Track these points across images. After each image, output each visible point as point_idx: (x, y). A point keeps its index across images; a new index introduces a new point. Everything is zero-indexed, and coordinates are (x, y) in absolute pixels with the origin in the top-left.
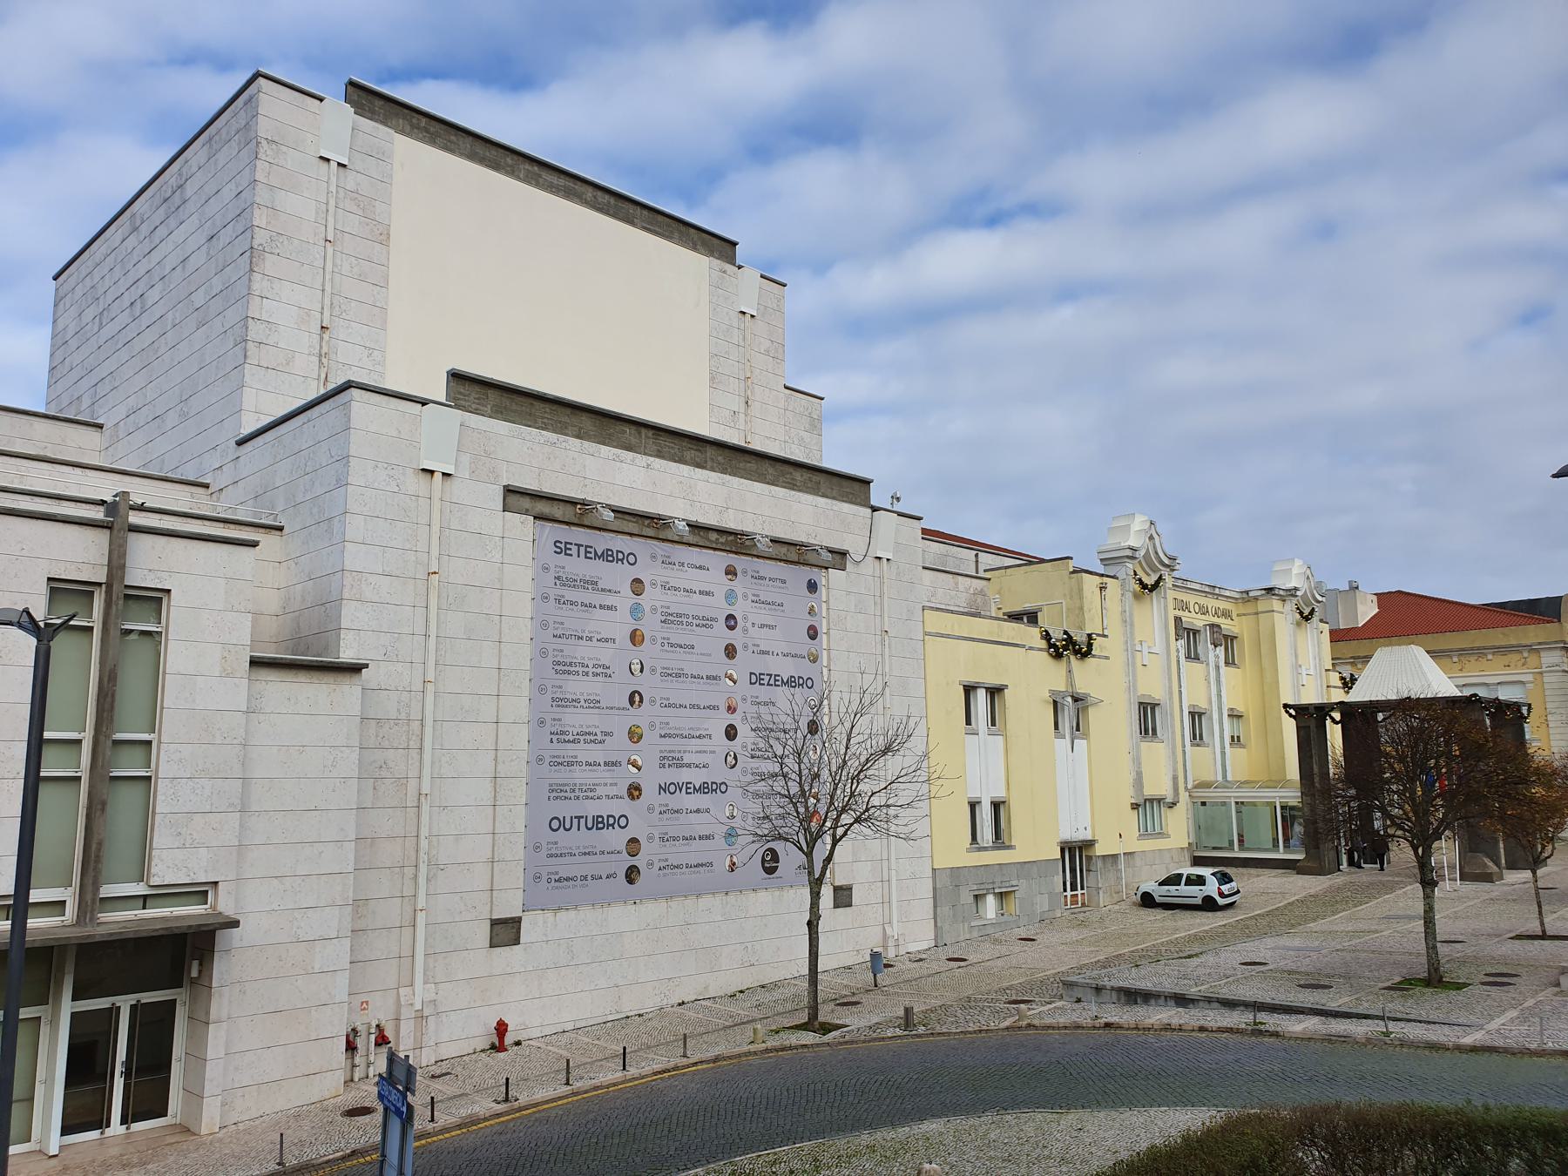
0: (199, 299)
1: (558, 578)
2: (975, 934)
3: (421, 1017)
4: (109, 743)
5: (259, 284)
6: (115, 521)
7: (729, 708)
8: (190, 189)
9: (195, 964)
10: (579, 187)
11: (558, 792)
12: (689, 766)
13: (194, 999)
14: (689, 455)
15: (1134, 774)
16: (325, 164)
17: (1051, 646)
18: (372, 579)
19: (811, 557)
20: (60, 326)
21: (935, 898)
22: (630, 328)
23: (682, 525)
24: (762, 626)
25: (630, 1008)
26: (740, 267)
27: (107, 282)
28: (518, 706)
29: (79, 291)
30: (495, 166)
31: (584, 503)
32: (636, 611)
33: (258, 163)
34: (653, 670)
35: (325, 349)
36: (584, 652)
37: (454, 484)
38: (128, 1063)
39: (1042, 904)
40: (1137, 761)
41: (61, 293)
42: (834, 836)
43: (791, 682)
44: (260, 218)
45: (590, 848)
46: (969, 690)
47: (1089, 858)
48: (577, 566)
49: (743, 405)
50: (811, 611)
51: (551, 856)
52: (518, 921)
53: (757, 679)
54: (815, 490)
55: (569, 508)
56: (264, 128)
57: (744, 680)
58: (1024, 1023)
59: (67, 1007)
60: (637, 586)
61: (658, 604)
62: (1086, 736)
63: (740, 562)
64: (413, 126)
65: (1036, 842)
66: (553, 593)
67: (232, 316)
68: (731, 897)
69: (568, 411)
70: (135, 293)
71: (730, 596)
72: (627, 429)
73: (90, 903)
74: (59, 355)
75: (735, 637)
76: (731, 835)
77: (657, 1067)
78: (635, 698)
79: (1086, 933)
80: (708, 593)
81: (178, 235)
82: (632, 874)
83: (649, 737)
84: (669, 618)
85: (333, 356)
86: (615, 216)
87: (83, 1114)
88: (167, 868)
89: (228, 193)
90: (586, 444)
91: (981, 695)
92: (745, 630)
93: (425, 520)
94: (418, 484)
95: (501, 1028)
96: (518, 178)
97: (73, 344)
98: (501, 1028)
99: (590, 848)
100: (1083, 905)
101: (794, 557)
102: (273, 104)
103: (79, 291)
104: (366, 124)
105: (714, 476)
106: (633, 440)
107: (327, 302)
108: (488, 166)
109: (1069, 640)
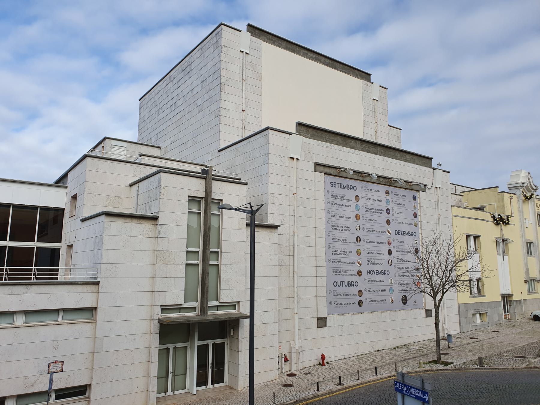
0: (199, 102)
1: (332, 195)
2: (474, 329)
3: (298, 352)
4: (209, 252)
5: (223, 96)
6: (206, 175)
7: (389, 243)
8: (193, 66)
9: (232, 330)
10: (320, 57)
11: (336, 272)
12: (376, 264)
13: (231, 343)
14: (372, 149)
15: (525, 269)
16: (241, 53)
17: (495, 220)
18: (277, 196)
19: (415, 187)
20: (142, 115)
21: (459, 314)
22: (342, 105)
23: (374, 175)
24: (399, 213)
25: (362, 351)
26: (372, 83)
27: (161, 100)
28: (322, 242)
29: (149, 103)
30: (293, 51)
31: (340, 168)
32: (357, 207)
33: (222, 54)
34: (363, 229)
35: (244, 118)
36: (340, 222)
37: (300, 161)
38: (212, 364)
39: (496, 318)
40: (526, 264)
41: (142, 105)
42: (443, 292)
43: (409, 234)
44: (223, 73)
45: (349, 293)
46: (468, 236)
47: (510, 301)
48: (338, 191)
49: (375, 132)
50: (414, 207)
51: (334, 295)
52: (325, 318)
53: (398, 233)
54: (414, 162)
55: (335, 170)
56: (224, 42)
57: (393, 233)
58: (533, 366)
59: (197, 343)
60: (357, 198)
61: (364, 205)
62: (508, 254)
63: (390, 189)
64: (268, 39)
65: (492, 295)
66: (331, 201)
67: (214, 107)
68: (392, 313)
69: (334, 135)
70: (172, 102)
71: (387, 201)
72: (352, 141)
73: (204, 308)
74: (142, 126)
75: (390, 217)
76: (391, 290)
77: (388, 375)
78: (358, 239)
79: (514, 330)
80: (380, 201)
81: (189, 81)
82: (360, 303)
83: (364, 253)
84: (368, 210)
85: (246, 120)
86: (331, 67)
87: (202, 381)
88: (226, 296)
89: (210, 65)
90: (339, 147)
91: (472, 239)
92: (393, 214)
93: (291, 175)
94: (289, 162)
95: (323, 357)
96: (301, 55)
97: (148, 121)
98: (323, 357)
99: (349, 293)
100: (509, 319)
101: (408, 187)
102: (225, 32)
103: (149, 103)
104: (254, 39)
105: (381, 157)
106: (354, 145)
107: (244, 101)
108: (291, 51)
109: (502, 219)
